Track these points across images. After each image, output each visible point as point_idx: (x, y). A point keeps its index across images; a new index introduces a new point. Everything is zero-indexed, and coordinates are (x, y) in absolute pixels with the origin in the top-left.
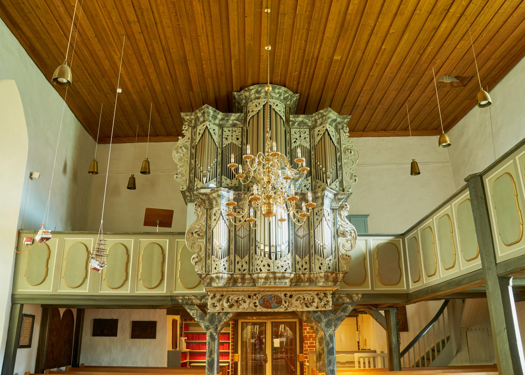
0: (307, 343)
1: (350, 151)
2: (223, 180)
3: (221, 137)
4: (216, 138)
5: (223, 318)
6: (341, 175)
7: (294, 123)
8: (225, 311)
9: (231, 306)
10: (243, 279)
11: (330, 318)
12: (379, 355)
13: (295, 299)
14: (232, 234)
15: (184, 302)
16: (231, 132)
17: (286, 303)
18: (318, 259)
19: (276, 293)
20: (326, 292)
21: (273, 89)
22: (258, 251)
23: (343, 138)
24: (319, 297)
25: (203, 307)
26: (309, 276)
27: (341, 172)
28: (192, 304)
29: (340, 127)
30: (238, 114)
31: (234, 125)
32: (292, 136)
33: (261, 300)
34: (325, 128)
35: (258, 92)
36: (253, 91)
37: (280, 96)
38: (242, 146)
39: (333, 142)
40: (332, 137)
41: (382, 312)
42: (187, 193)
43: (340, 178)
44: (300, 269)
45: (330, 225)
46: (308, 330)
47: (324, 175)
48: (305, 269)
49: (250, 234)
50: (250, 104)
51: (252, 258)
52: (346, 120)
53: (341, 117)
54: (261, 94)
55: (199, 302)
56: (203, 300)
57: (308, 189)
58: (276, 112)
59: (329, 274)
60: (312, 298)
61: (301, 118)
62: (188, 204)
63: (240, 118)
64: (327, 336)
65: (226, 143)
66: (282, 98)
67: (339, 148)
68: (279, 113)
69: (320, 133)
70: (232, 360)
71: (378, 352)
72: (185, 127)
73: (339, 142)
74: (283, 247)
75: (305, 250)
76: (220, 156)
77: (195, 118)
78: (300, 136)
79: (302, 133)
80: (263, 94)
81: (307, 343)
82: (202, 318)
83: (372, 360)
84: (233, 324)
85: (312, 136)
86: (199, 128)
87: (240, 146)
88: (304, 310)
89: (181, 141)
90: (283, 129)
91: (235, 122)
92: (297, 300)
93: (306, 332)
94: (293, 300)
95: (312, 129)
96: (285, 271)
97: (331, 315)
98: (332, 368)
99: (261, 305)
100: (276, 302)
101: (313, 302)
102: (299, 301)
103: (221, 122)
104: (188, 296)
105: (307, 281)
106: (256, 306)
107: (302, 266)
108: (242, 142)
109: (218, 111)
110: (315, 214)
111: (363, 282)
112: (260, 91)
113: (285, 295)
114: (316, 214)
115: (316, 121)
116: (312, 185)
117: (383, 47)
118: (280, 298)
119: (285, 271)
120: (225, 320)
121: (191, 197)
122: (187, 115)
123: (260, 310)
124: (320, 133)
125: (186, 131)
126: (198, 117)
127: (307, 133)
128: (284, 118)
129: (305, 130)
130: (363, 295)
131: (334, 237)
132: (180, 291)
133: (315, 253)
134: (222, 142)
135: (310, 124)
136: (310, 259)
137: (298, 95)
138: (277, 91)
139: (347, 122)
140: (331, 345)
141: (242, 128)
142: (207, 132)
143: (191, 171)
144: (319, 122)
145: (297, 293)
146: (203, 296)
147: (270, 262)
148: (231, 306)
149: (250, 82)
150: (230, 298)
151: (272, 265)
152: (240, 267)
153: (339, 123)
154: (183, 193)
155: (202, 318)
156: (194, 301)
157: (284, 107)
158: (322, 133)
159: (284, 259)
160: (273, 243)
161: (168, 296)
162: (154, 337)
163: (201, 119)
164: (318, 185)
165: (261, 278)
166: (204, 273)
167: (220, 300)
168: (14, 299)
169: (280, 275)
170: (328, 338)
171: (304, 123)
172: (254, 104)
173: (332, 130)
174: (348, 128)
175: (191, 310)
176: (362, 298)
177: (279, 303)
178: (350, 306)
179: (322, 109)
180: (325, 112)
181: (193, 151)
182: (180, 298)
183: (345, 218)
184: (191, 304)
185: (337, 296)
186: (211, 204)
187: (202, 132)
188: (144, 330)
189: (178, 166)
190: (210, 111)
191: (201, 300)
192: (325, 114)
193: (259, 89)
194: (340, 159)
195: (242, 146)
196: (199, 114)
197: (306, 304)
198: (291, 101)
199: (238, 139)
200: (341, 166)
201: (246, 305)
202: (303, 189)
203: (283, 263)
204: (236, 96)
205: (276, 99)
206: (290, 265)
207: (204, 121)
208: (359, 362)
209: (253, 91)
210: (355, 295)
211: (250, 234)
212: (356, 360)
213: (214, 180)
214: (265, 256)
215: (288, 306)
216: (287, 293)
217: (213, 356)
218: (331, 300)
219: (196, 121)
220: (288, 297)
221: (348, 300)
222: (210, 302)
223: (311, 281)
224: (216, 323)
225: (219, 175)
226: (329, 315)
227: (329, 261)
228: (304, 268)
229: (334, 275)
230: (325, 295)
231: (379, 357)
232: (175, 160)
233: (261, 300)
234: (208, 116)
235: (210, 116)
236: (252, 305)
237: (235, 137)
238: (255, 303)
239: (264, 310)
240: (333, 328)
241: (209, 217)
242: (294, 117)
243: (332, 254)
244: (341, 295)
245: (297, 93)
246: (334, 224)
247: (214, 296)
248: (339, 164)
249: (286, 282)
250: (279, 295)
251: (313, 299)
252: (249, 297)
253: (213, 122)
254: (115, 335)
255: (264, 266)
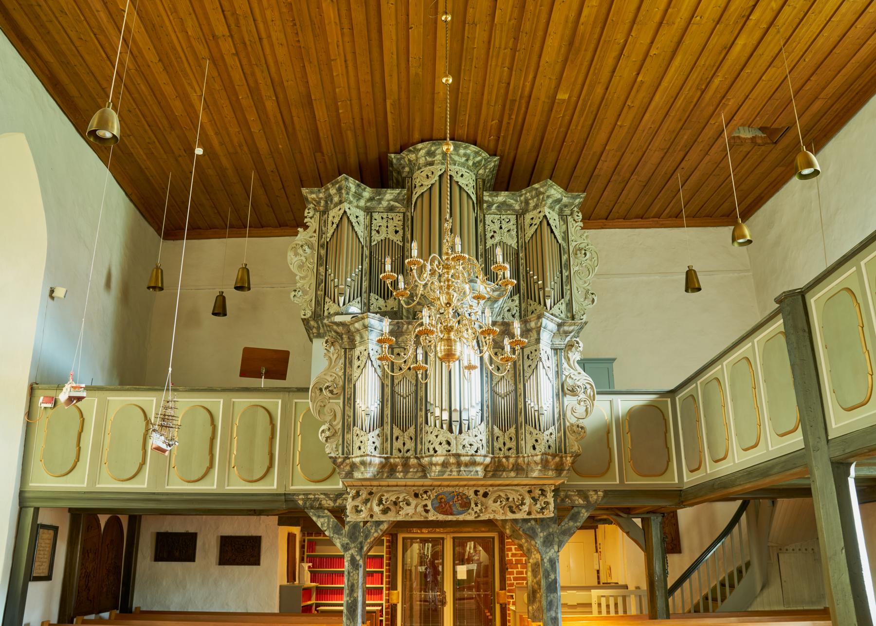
0: (512, 573)
1: (583, 252)
2: (373, 300)
3: (369, 228)
4: (360, 230)
5: (373, 531)
6: (569, 292)
7: (490, 205)
8: (375, 519)
9: (385, 511)
10: (406, 465)
11: (551, 530)
12: (632, 592)
13: (492, 499)
14: (388, 391)
15: (308, 504)
16: (385, 220)
17: (476, 505)
18: (531, 433)
19: (461, 489)
20: (543, 488)
21: (456, 148)
22: (431, 419)
23: (572, 230)
24: (533, 495)
25: (339, 513)
26: (516, 461)
27: (569, 287)
28: (321, 508)
29: (567, 211)
30: (397, 191)
31: (391, 209)
32: (487, 227)
33: (436, 501)
34: (542, 214)
35: (430, 154)
36: (422, 153)
37: (467, 160)
38: (404, 244)
39: (555, 237)
40: (553, 228)
41: (638, 521)
42: (312, 323)
43: (567, 297)
44: (500, 449)
45: (551, 376)
46: (514, 552)
47: (541, 293)
48: (509, 449)
49: (417, 391)
50: (417, 174)
51: (421, 430)
52: (577, 201)
53: (569, 195)
54: (435, 156)
55: (332, 504)
56: (339, 501)
57: (513, 316)
58: (460, 187)
59: (549, 457)
60: (520, 498)
61: (502, 197)
62: (314, 340)
63: (401, 197)
64: (545, 560)
65: (376, 238)
66: (470, 163)
67: (566, 247)
68: (466, 189)
69: (534, 222)
70: (388, 601)
71: (631, 587)
72: (309, 213)
73: (566, 237)
74: (473, 413)
75: (509, 418)
76: (367, 260)
77: (326, 197)
78: (501, 228)
79: (503, 222)
80: (439, 157)
81: (512, 573)
82: (337, 530)
83: (620, 601)
84: (388, 541)
85: (520, 228)
86: (332, 213)
87: (401, 244)
88: (507, 518)
89: (302, 235)
90: (473, 216)
91: (392, 203)
92: (495, 501)
93: (510, 554)
94: (490, 501)
95: (520, 215)
96: (476, 452)
97: (553, 526)
98: (554, 615)
99: (435, 509)
100: (461, 504)
101: (523, 504)
102: (499, 503)
103: (368, 204)
104: (314, 495)
105: (512, 470)
106: (427, 511)
107: (504, 444)
108: (403, 238)
109: (363, 186)
110: (526, 357)
111: (605, 470)
112: (434, 152)
113: (476, 492)
114: (528, 358)
115: (527, 202)
116: (520, 309)
117: (640, 78)
118: (467, 497)
119: (476, 452)
120: (376, 535)
121: (318, 328)
122: (312, 193)
123: (434, 518)
124: (534, 222)
125: (311, 218)
126: (330, 195)
127: (512, 223)
128: (474, 197)
129: (509, 217)
130: (606, 492)
131: (558, 395)
132: (300, 485)
133: (526, 422)
134: (371, 237)
135: (517, 207)
136: (517, 432)
137: (497, 158)
138: (462, 151)
139: (580, 203)
140: (552, 577)
141: (404, 213)
142: (345, 220)
143: (320, 285)
144: (532, 203)
145: (496, 488)
146: (339, 495)
147: (451, 437)
148: (385, 511)
149: (417, 136)
150: (384, 498)
151: (453, 442)
152: (401, 446)
153: (566, 206)
154: (305, 322)
155: (337, 530)
156: (324, 502)
157: (474, 178)
158: (537, 221)
159: (473, 432)
160: (456, 405)
161: (280, 495)
162: (257, 562)
163: (336, 199)
164: (530, 309)
165: (435, 465)
166: (340, 455)
167: (366, 501)
168: (23, 500)
169: (468, 458)
170: (547, 565)
171: (507, 205)
172: (424, 174)
173: (553, 217)
174: (580, 214)
175: (319, 517)
176: (604, 497)
177: (466, 505)
178: (583, 511)
179: (538, 182)
180: (542, 187)
181: (323, 252)
182: (301, 497)
183: (576, 364)
184: (318, 508)
185: (562, 494)
186: (352, 341)
187: (336, 220)
188: (241, 551)
189: (298, 278)
190: (351, 185)
191: (335, 501)
192: (542, 190)
193: (433, 149)
194: (568, 266)
195: (404, 244)
196: (333, 191)
197: (510, 508)
198: (485, 169)
199: (396, 232)
200: (569, 277)
201: (410, 510)
202: (506, 316)
203: (472, 440)
204: (394, 161)
205: (461, 165)
206: (484, 442)
207: (341, 202)
208: (599, 605)
209: (422, 153)
210: (592, 493)
211: (417, 391)
212: (594, 601)
213: (356, 300)
214: (442, 427)
215: (481, 510)
216: (478, 489)
217: (355, 595)
218: (551, 501)
219: (326, 202)
220: (480, 497)
221: (581, 502)
222: (350, 504)
223: (518, 469)
224: (360, 539)
225: (365, 292)
226: (549, 526)
227: (549, 436)
228: (507, 447)
229: (557, 459)
230: (543, 493)
231: (633, 597)
232: (291, 267)
233: (436, 501)
234: (348, 194)
235: (351, 193)
236: (420, 509)
237: (391, 229)
238: (426, 506)
239: (441, 517)
240: (556, 547)
241: (348, 363)
242: (490, 196)
243: (554, 424)
244: (570, 493)
245: (495, 155)
246: (558, 374)
247: (358, 494)
248: (566, 274)
249: (477, 472)
250: (466, 492)
251: (523, 499)
252: (416, 495)
253: (355, 204)
254: (192, 559)
255: (441, 444)
